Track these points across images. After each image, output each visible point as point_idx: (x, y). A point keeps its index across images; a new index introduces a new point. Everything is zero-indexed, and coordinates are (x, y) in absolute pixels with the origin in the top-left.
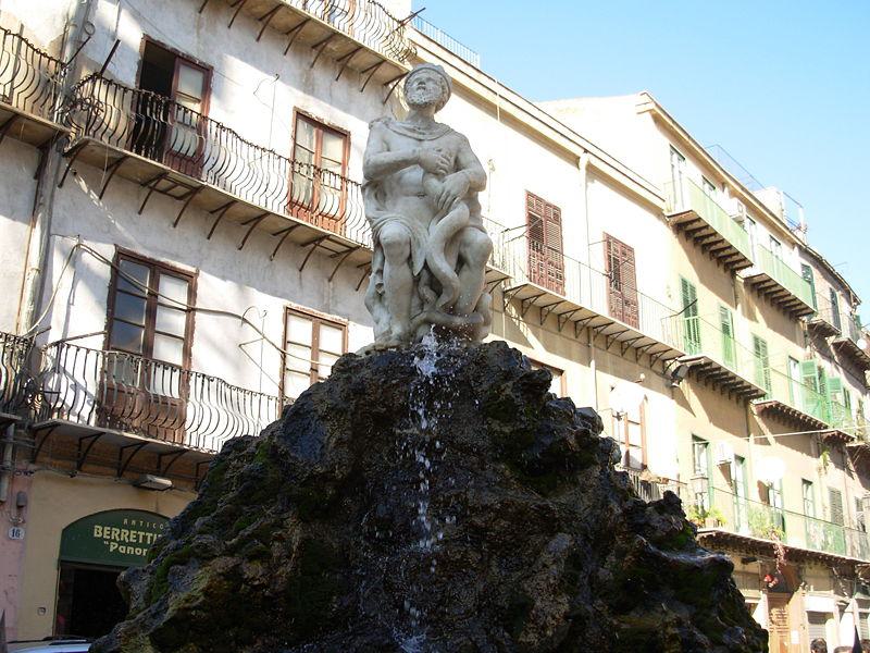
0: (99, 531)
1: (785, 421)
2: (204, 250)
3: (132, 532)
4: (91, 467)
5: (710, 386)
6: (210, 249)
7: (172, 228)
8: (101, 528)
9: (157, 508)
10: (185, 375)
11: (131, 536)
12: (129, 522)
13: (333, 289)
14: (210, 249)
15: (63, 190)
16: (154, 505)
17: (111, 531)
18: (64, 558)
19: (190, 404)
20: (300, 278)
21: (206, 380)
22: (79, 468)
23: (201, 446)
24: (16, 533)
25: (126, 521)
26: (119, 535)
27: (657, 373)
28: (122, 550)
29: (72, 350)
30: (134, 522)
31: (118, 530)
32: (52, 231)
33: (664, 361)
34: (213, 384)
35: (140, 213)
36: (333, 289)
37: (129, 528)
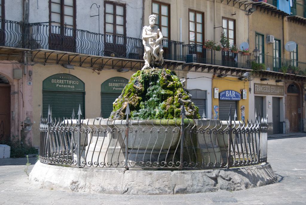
1: (296, 22)
3: (71, 81)
5: (266, 12)
8: (53, 80)
10: (75, 30)
11: (63, 82)
12: (62, 77)
17: (56, 81)
19: (104, 43)
22: (46, 62)
24: (30, 83)
25: (60, 77)
26: (59, 82)
27: (242, 10)
28: (116, 89)
29: (42, 27)
30: (63, 77)
31: (58, 80)
33: (245, 5)
34: (85, 33)
37: (62, 79)
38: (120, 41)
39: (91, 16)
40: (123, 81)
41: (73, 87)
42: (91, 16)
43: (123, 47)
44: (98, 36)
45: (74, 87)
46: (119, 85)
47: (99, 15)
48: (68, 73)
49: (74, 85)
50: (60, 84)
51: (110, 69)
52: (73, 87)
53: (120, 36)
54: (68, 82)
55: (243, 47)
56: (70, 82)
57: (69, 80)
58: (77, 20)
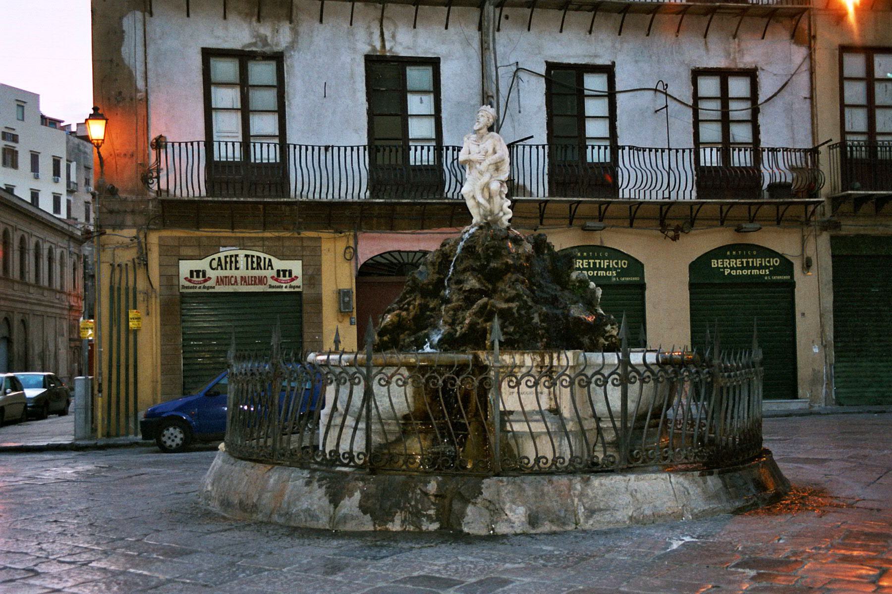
0: (714, 263)
2: (618, 45)
3: (585, 261)
4: (551, 221)
6: (622, 43)
7: (588, 36)
9: (602, 242)
11: (585, 264)
12: (582, 254)
13: (739, 45)
14: (622, 43)
15: (501, 33)
16: (599, 240)
17: (723, 262)
18: (693, 281)
20: (706, 43)
21: (636, 152)
23: (637, 197)
26: (729, 264)
28: (734, 273)
32: (498, 65)
34: (780, 154)
35: (561, 31)
36: (739, 45)
37: (729, 258)
38: (741, 159)
39: (656, 112)
40: (755, 253)
41: (612, 274)
42: (656, 112)
43: (753, 174)
44: (641, 153)
45: (768, 273)
46: (742, 263)
47: (667, 106)
48: (599, 244)
49: (615, 269)
50: (729, 266)
51: (716, 226)
52: (612, 274)
53: (741, 145)
54: (600, 263)
55: (421, 102)
56: (605, 264)
57: (604, 258)
58: (617, 123)
